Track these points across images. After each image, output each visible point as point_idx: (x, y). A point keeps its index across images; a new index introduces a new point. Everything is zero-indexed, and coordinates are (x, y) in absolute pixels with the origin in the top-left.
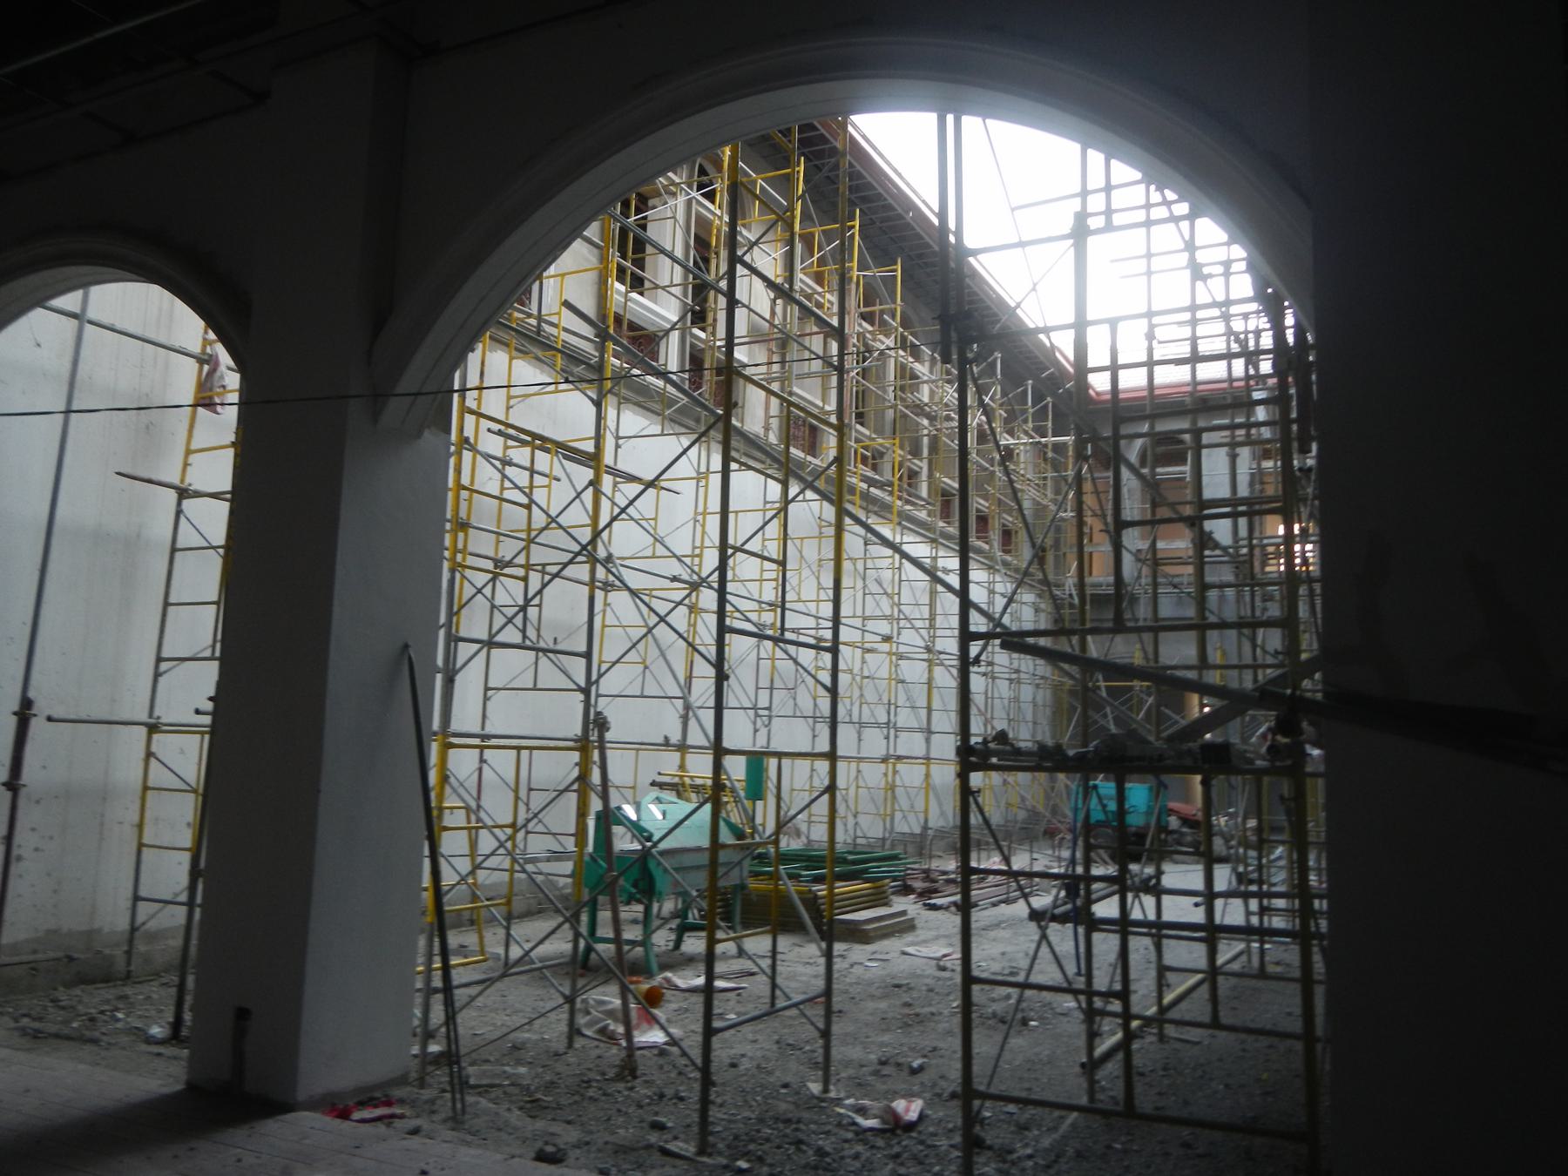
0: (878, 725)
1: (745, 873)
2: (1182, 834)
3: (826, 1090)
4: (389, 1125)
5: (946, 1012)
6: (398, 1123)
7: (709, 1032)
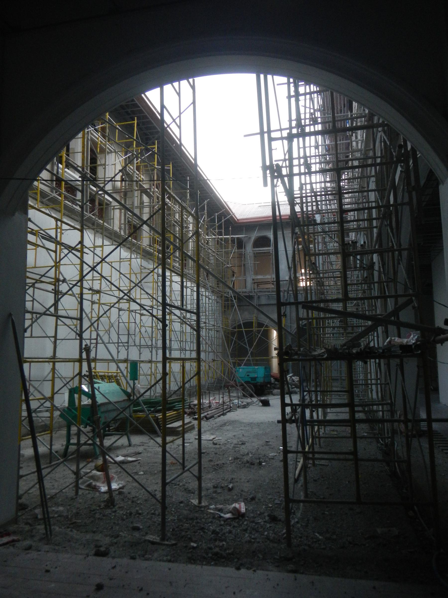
0: (147, 346)
1: (132, 411)
2: (275, 384)
3: (200, 502)
4: (13, 546)
5: (228, 462)
6: (18, 544)
7: (164, 484)
